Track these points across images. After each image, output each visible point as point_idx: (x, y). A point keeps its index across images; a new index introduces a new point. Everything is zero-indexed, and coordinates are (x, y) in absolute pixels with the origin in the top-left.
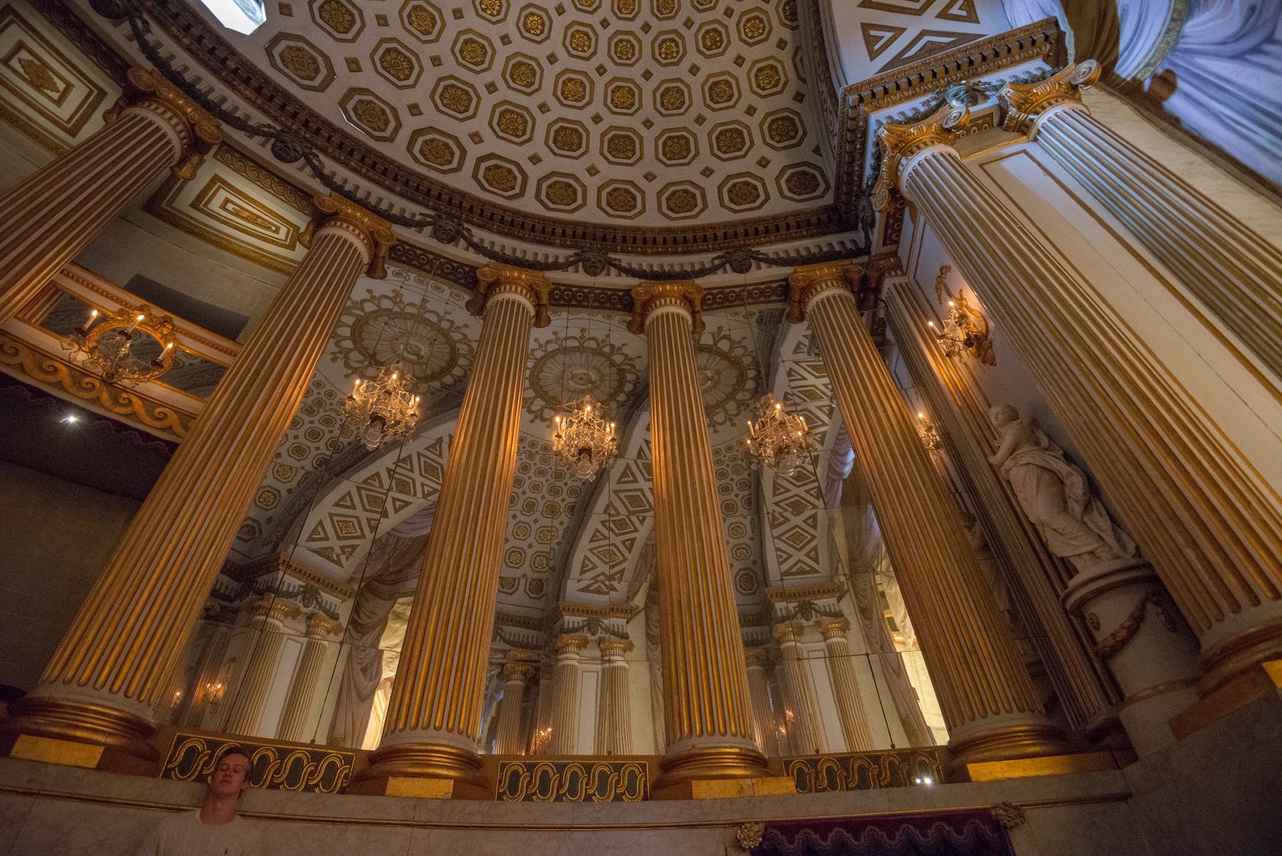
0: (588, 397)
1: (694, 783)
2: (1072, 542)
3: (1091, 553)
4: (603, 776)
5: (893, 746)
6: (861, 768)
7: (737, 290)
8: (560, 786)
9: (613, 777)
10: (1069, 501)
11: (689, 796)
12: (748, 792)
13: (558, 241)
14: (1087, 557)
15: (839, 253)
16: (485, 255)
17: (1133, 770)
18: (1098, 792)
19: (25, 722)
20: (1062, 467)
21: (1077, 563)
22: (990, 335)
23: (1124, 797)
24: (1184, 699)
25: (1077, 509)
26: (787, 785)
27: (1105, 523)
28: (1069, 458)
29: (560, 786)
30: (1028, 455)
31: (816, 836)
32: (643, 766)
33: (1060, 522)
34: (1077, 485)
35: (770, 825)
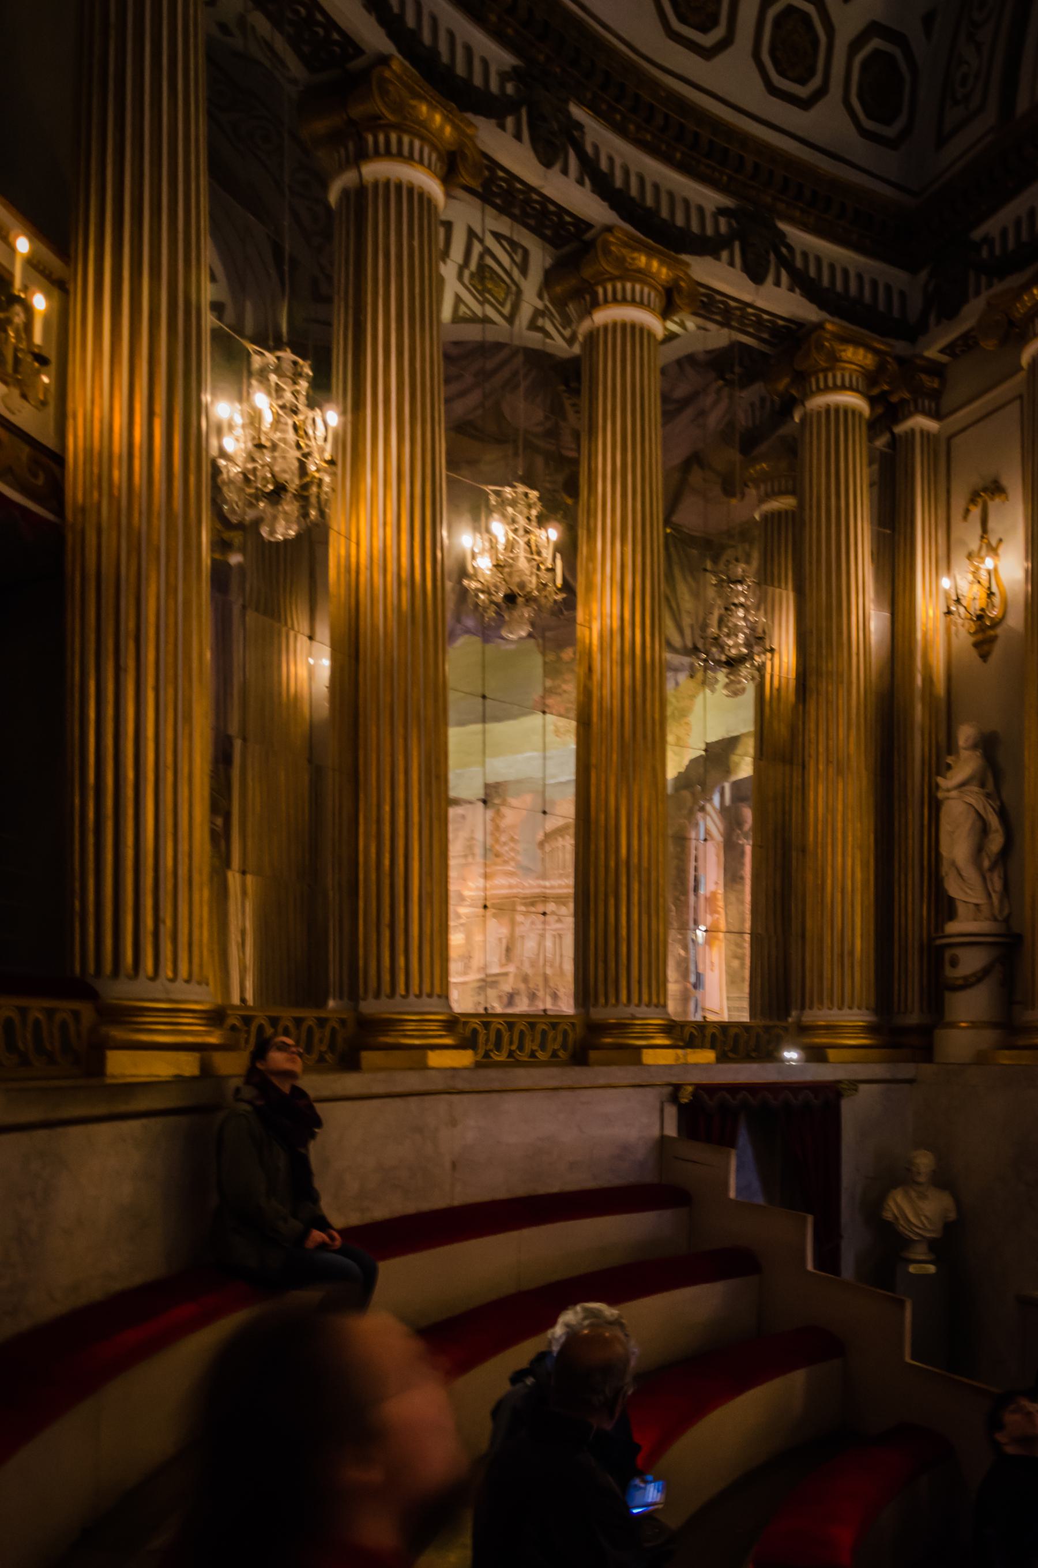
0: (562, 512)
1: (645, 1051)
2: (968, 891)
3: (977, 905)
4: (544, 1033)
5: (456, 802)
6: (736, 1035)
7: (733, 304)
8: (511, 1043)
9: (551, 1034)
10: (984, 854)
11: (638, 1061)
12: (682, 1061)
13: (493, 18)
14: (972, 907)
15: (685, 232)
16: (392, 35)
17: (927, 1068)
18: (900, 1076)
19: (118, 1034)
20: (994, 821)
21: (961, 909)
22: (999, 631)
23: (910, 1081)
24: (987, 1037)
25: (986, 864)
26: (708, 1056)
27: (997, 884)
28: (1003, 814)
29: (511, 1043)
30: (974, 797)
31: (728, 1096)
32: (573, 1024)
33: (970, 873)
34: (996, 842)
35: (698, 1087)
